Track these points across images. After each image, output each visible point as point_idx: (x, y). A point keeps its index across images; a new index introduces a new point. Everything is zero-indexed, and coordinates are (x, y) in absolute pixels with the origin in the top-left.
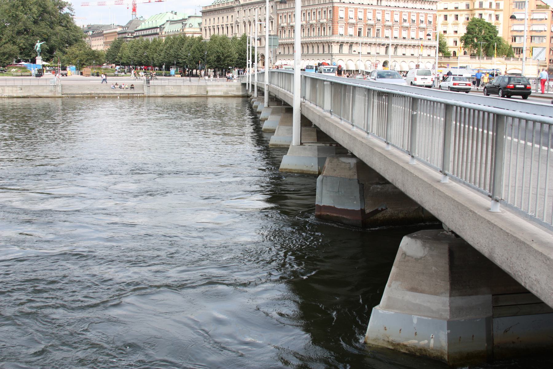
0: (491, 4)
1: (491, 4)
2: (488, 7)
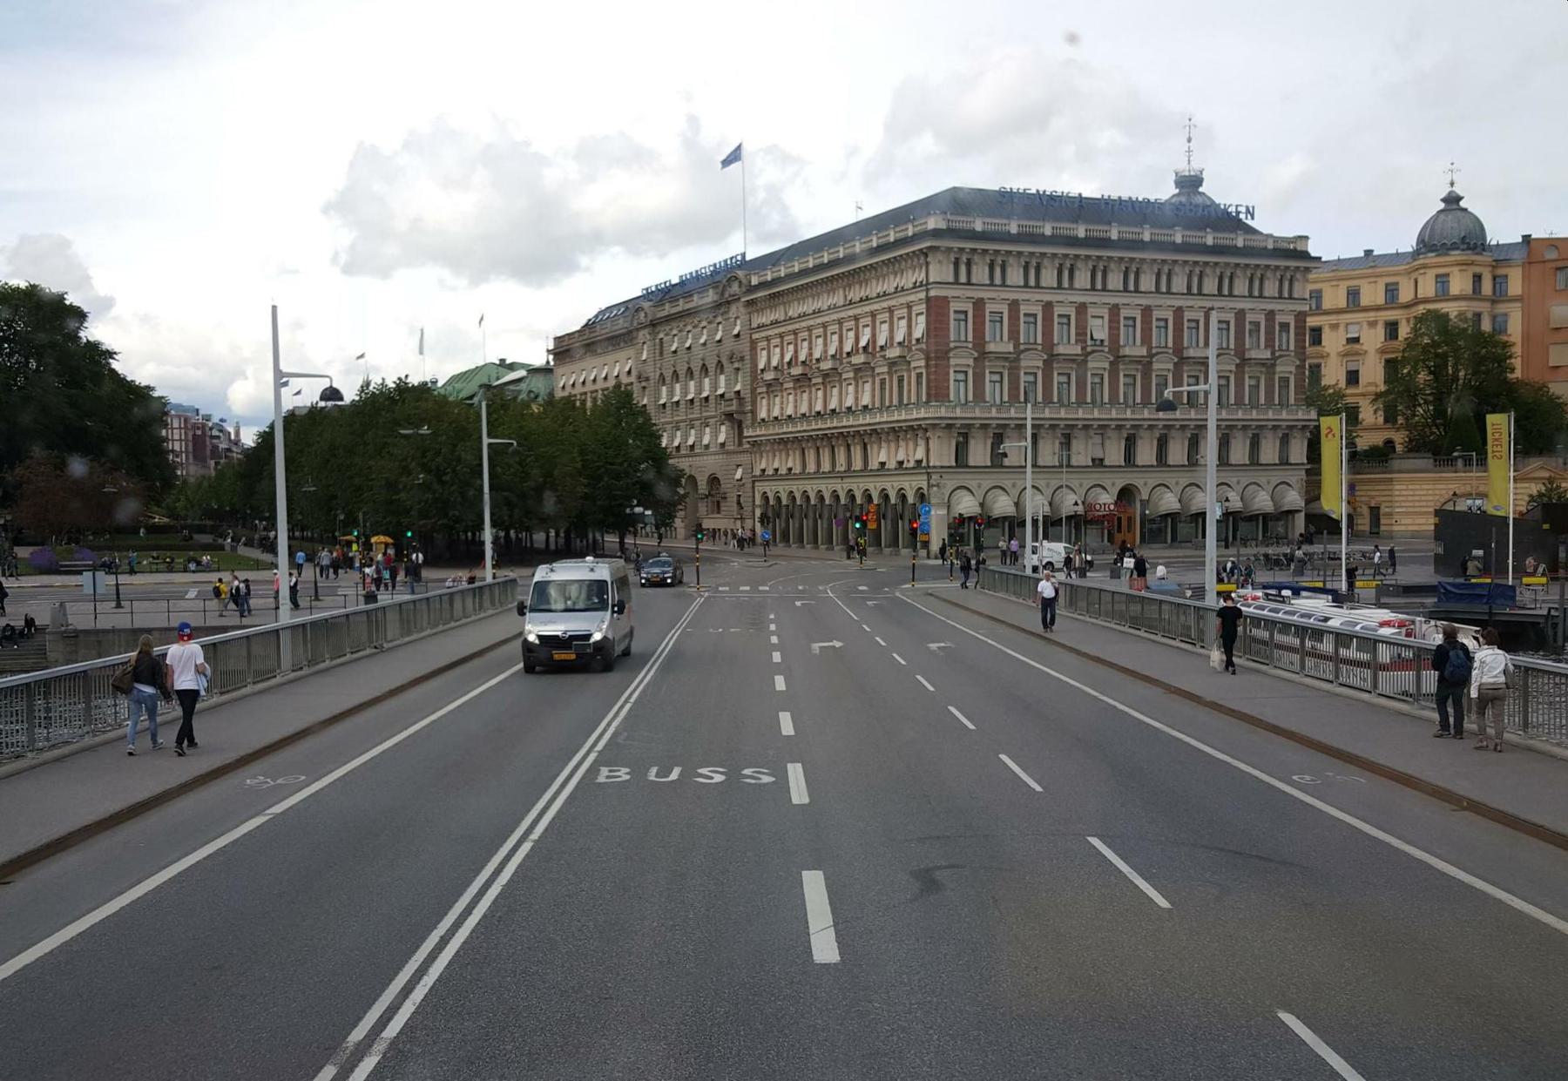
0: (1477, 278)
1: (1477, 278)
2: (1469, 289)
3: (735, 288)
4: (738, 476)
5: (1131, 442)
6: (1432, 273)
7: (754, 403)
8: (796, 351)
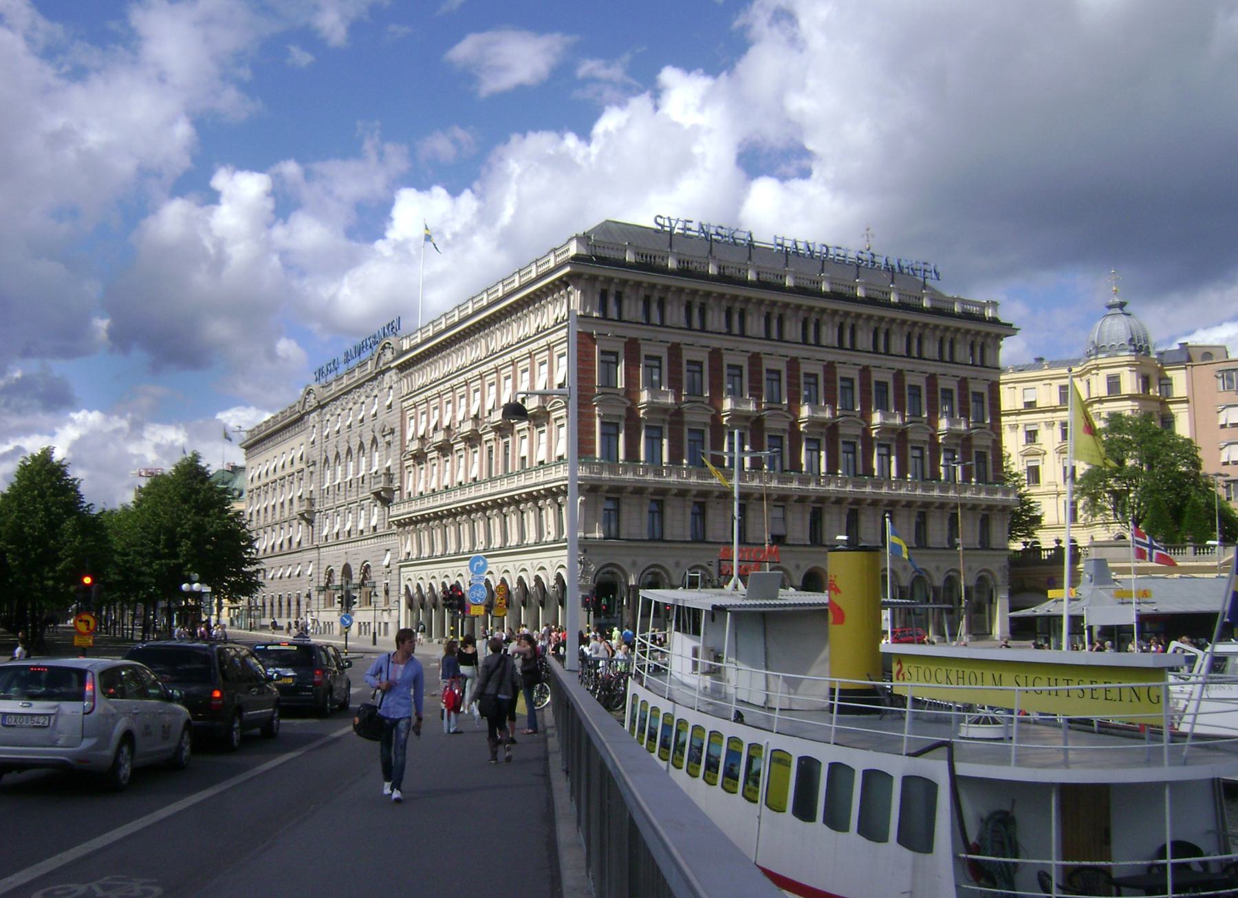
3: (389, 355)
4: (386, 563)
5: (816, 519)
6: (1104, 374)
7: (402, 478)
8: (441, 416)
